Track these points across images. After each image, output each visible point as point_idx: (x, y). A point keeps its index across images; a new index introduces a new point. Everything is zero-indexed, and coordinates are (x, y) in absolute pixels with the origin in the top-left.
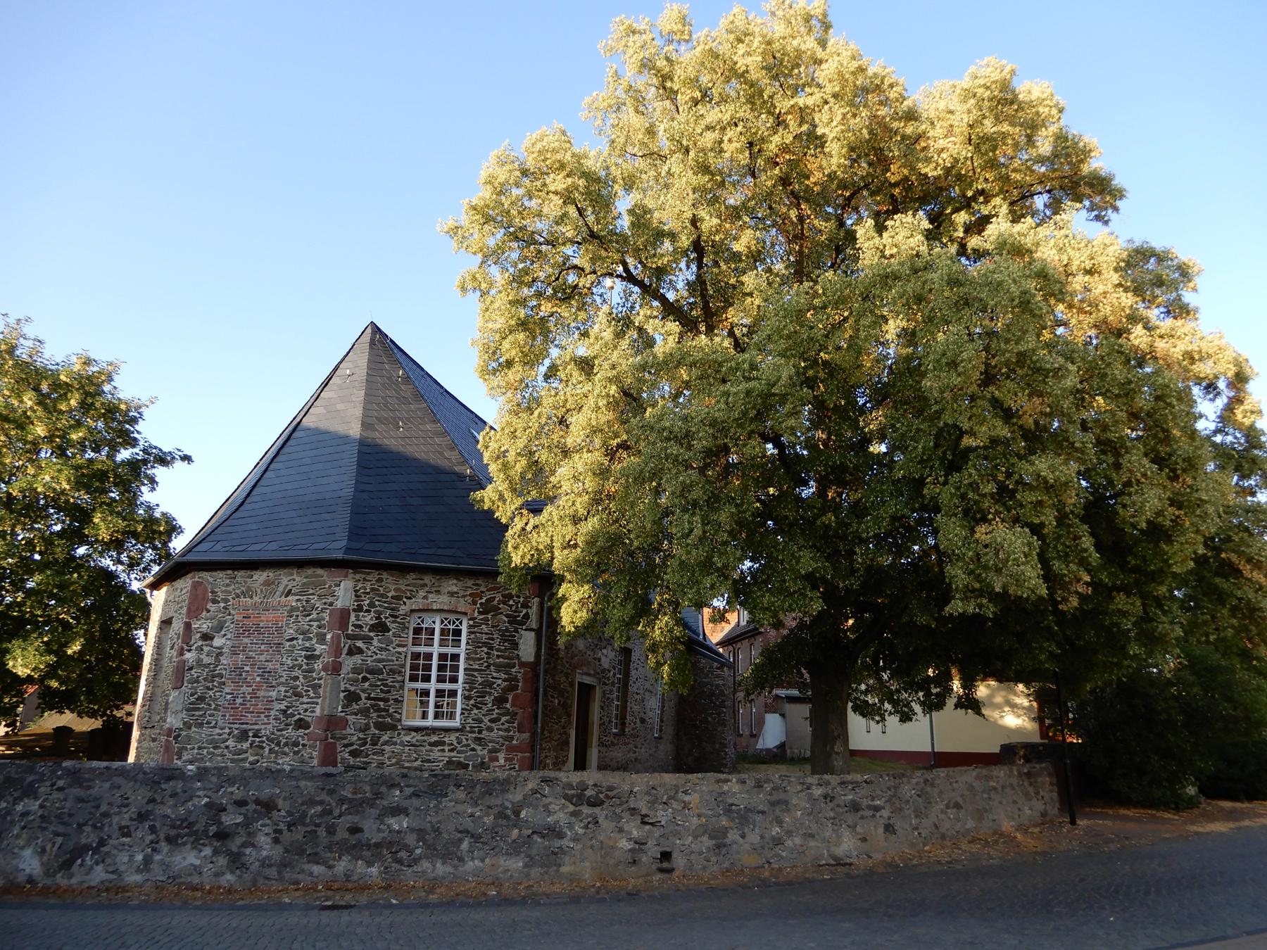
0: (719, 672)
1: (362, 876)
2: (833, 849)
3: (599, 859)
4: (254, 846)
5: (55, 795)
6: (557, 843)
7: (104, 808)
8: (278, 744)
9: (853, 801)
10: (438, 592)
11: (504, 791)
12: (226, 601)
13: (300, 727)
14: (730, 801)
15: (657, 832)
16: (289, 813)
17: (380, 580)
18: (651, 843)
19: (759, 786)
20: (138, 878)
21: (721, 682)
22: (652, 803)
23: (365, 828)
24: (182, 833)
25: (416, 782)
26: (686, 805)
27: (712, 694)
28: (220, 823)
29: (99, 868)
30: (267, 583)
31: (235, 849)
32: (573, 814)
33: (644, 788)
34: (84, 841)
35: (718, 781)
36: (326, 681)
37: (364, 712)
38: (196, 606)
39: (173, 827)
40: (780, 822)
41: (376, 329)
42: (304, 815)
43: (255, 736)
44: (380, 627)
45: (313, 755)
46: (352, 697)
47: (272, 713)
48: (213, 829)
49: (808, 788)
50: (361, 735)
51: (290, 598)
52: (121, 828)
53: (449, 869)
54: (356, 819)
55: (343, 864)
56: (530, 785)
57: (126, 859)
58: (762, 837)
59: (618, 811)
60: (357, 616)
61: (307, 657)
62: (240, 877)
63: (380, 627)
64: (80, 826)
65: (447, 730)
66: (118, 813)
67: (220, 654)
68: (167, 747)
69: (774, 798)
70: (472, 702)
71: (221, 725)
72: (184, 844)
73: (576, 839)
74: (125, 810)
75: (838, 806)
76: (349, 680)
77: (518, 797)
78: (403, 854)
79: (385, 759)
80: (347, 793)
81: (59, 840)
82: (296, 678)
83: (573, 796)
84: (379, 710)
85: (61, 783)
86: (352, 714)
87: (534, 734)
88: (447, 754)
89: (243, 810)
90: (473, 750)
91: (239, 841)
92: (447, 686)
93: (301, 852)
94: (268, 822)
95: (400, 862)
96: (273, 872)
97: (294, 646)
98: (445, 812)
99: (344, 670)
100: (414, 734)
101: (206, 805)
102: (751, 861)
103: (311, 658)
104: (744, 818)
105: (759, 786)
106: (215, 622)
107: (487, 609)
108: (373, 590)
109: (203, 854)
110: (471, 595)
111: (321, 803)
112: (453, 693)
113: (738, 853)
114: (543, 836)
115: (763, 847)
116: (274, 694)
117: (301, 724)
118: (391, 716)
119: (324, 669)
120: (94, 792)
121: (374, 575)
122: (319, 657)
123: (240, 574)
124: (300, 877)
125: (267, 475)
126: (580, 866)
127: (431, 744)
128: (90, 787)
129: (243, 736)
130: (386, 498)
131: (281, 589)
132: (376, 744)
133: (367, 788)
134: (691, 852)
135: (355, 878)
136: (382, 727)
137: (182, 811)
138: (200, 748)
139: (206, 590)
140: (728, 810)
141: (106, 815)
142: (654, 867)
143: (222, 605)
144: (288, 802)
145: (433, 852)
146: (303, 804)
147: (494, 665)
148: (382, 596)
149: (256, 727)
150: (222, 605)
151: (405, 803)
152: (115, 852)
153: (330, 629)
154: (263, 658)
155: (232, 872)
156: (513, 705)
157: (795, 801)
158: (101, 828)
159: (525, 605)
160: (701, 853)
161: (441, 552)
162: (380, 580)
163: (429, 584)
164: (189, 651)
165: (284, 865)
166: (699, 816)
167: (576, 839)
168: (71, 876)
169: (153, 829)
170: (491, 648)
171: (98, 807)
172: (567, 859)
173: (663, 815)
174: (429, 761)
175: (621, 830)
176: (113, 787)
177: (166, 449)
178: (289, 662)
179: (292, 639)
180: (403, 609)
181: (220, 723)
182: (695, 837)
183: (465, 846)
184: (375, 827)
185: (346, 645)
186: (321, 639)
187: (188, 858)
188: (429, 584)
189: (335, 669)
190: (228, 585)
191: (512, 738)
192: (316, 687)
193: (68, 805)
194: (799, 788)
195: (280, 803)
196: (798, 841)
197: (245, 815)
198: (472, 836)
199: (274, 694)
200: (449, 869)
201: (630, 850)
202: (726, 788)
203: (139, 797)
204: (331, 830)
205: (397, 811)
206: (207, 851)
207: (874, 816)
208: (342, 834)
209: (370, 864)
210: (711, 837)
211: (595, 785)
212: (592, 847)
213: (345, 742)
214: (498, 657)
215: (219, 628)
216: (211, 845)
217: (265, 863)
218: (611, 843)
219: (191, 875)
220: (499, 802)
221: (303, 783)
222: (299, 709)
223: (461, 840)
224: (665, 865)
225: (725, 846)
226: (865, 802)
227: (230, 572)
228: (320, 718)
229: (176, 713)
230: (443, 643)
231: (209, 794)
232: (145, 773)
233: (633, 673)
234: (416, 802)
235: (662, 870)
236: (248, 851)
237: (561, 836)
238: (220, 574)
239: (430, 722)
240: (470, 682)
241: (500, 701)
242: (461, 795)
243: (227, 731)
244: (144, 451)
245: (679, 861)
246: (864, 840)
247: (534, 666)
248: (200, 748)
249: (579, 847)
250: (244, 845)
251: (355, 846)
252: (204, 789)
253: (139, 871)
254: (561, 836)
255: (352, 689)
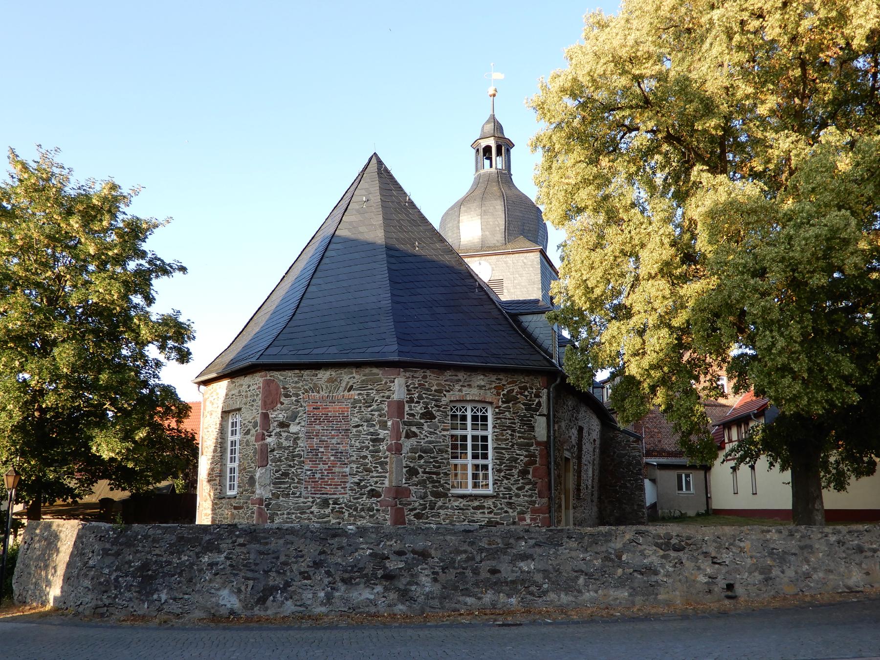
0: (635, 445)
1: (505, 605)
2: (846, 580)
3: (685, 589)
4: (417, 584)
5: (238, 550)
6: (654, 578)
7: (283, 558)
8: (356, 509)
9: (858, 545)
10: (470, 386)
11: (607, 541)
12: (297, 395)
13: (373, 496)
14: (772, 546)
15: (724, 570)
16: (441, 560)
17: (425, 377)
18: (720, 577)
19: (791, 535)
20: (323, 609)
21: (637, 454)
22: (718, 548)
23: (502, 570)
24: (353, 576)
25: (536, 536)
26: (742, 550)
27: (630, 464)
28: (385, 568)
29: (289, 603)
30: (331, 380)
31: (402, 587)
32: (663, 557)
33: (712, 538)
34: (271, 583)
35: (763, 532)
36: (390, 458)
37: (422, 483)
38: (271, 399)
39: (346, 571)
40: (808, 561)
41: (380, 162)
42: (453, 561)
43: (335, 503)
44: (428, 415)
45: (386, 518)
46: (412, 472)
47: (348, 485)
48: (380, 573)
49: (826, 536)
50: (422, 502)
51: (352, 392)
52: (301, 573)
53: (571, 598)
54: (494, 563)
55: (489, 596)
56: (628, 537)
57: (310, 596)
58: (796, 573)
59: (695, 554)
60: (410, 407)
61: (373, 440)
62: (410, 607)
63: (428, 415)
64: (266, 572)
65: (486, 497)
66: (296, 562)
67: (298, 438)
68: (261, 514)
69: (802, 544)
70: (503, 474)
71: (305, 496)
72: (358, 584)
73: (668, 575)
74: (302, 560)
75: (848, 549)
76: (409, 458)
77: (619, 545)
78: (533, 589)
79: (441, 520)
80: (484, 544)
81: (251, 583)
82: (365, 457)
83: (662, 544)
84: (433, 482)
85: (241, 541)
86: (413, 485)
87: (550, 499)
88: (487, 515)
89: (403, 558)
90: (506, 512)
91: (404, 581)
92: (480, 462)
93: (456, 588)
94: (426, 566)
95: (532, 594)
96: (436, 603)
97: (360, 432)
98: (563, 557)
99: (404, 451)
100: (461, 500)
101: (371, 555)
102: (790, 590)
103: (376, 441)
104: (782, 558)
105: (791, 535)
106: (290, 413)
107: (508, 398)
108: (420, 385)
109: (375, 591)
110: (495, 388)
111: (465, 552)
112: (485, 467)
113: (781, 584)
114: (642, 574)
115: (797, 580)
116: (347, 470)
117: (373, 494)
118: (442, 486)
119: (389, 449)
120: (272, 546)
121: (420, 373)
122: (383, 440)
123: (306, 373)
124: (457, 606)
125: (310, 289)
126: (672, 594)
127: (474, 508)
128: (267, 544)
129: (325, 503)
130: (391, 302)
131: (344, 384)
132: (433, 509)
133: (499, 541)
134: (748, 584)
135: (500, 606)
136: (437, 495)
137: (350, 560)
138: (288, 514)
139: (278, 386)
140: (771, 553)
141: (285, 564)
142: (723, 594)
143: (294, 398)
144: (439, 552)
145: (557, 586)
146: (451, 553)
147: (517, 444)
148: (428, 390)
149: (335, 496)
150: (294, 398)
151: (530, 551)
152: (300, 591)
153: (390, 417)
154: (334, 441)
155: (403, 603)
156: (533, 477)
157: (817, 546)
158: (284, 573)
159: (537, 396)
160: (754, 585)
161: (471, 353)
162: (425, 377)
163: (463, 380)
164: (270, 436)
165: (443, 598)
166: (751, 557)
167: (668, 575)
168: (266, 609)
169: (329, 574)
170: (514, 431)
171: (278, 558)
172: (662, 590)
173: (726, 557)
174: (474, 521)
175: (699, 568)
176: (287, 543)
177: (167, 261)
178: (357, 444)
179: (358, 426)
180: (444, 400)
181: (304, 493)
182: (750, 573)
183: (581, 581)
184: (509, 569)
185: (404, 430)
186: (384, 425)
187: (363, 594)
188: (463, 380)
189: (397, 449)
190: (296, 382)
191: (535, 502)
192: (383, 464)
193: (252, 556)
194: (820, 536)
195: (433, 552)
196: (821, 575)
197: (406, 562)
198: (586, 574)
199: (347, 470)
200: (571, 598)
201: (706, 583)
202: (768, 537)
203: (311, 550)
204: (476, 572)
205: (525, 557)
206: (379, 589)
207: (873, 556)
208: (484, 575)
209: (509, 596)
210: (761, 573)
211: (678, 536)
212: (680, 581)
213: (410, 507)
214: (520, 437)
215: (294, 417)
216: (381, 584)
217: (428, 596)
218: (693, 578)
219: (368, 606)
220: (604, 549)
221: (448, 538)
222: (372, 481)
223: (577, 578)
224: (730, 593)
225: (771, 579)
226: (867, 546)
227: (297, 371)
228: (389, 489)
229: (265, 486)
230: (475, 427)
231: (371, 547)
232: (312, 532)
233: (584, 447)
234: (538, 550)
235: (728, 597)
236: (413, 588)
237: (656, 573)
238: (289, 373)
239: (470, 490)
240: (500, 458)
241: (524, 473)
242: (573, 544)
243: (311, 499)
244: (150, 262)
245: (739, 590)
246: (868, 574)
247: (547, 444)
248: (288, 514)
249: (671, 581)
250: (410, 583)
251: (495, 583)
252: (367, 543)
253: (322, 604)
254: (656, 573)
255: (412, 465)
